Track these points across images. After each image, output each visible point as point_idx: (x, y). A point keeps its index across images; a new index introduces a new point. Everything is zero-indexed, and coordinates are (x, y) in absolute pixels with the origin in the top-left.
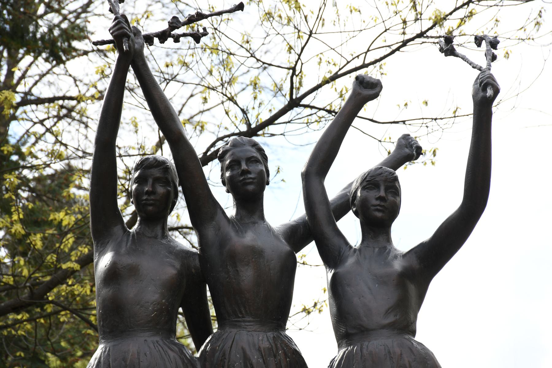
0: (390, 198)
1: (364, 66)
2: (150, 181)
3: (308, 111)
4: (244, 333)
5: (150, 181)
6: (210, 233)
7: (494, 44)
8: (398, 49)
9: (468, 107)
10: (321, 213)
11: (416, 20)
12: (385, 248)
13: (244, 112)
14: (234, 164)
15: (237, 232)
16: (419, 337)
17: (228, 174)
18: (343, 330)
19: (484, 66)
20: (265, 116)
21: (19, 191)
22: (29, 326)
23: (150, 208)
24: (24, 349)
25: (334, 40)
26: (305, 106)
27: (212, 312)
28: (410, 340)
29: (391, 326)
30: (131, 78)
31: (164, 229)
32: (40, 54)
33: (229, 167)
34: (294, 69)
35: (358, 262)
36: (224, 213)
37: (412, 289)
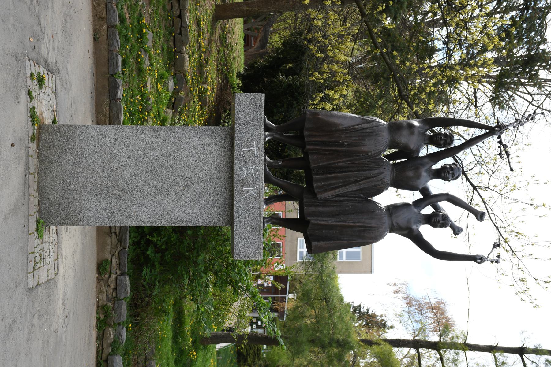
0: (439, 225)
1: (489, 213)
2: (445, 139)
3: (471, 192)
4: (390, 173)
5: (445, 139)
6: (426, 160)
7: (497, 262)
8: (495, 225)
9: (473, 253)
10: (434, 200)
11: (506, 232)
12: (420, 223)
13: (471, 169)
14: (452, 169)
15: (426, 170)
16: (388, 234)
17: (448, 166)
18: (391, 208)
19: (488, 259)
20: (469, 177)
22: (393, 94)
23: (435, 139)
24: (385, 93)
25: (499, 202)
26: (473, 192)
27: (398, 161)
28: (388, 231)
29: (392, 225)
30: (484, 131)
31: (427, 144)
32: (493, 93)
33: (450, 167)
34: (488, 188)
35: (415, 213)
36: (433, 165)
37: (406, 232)
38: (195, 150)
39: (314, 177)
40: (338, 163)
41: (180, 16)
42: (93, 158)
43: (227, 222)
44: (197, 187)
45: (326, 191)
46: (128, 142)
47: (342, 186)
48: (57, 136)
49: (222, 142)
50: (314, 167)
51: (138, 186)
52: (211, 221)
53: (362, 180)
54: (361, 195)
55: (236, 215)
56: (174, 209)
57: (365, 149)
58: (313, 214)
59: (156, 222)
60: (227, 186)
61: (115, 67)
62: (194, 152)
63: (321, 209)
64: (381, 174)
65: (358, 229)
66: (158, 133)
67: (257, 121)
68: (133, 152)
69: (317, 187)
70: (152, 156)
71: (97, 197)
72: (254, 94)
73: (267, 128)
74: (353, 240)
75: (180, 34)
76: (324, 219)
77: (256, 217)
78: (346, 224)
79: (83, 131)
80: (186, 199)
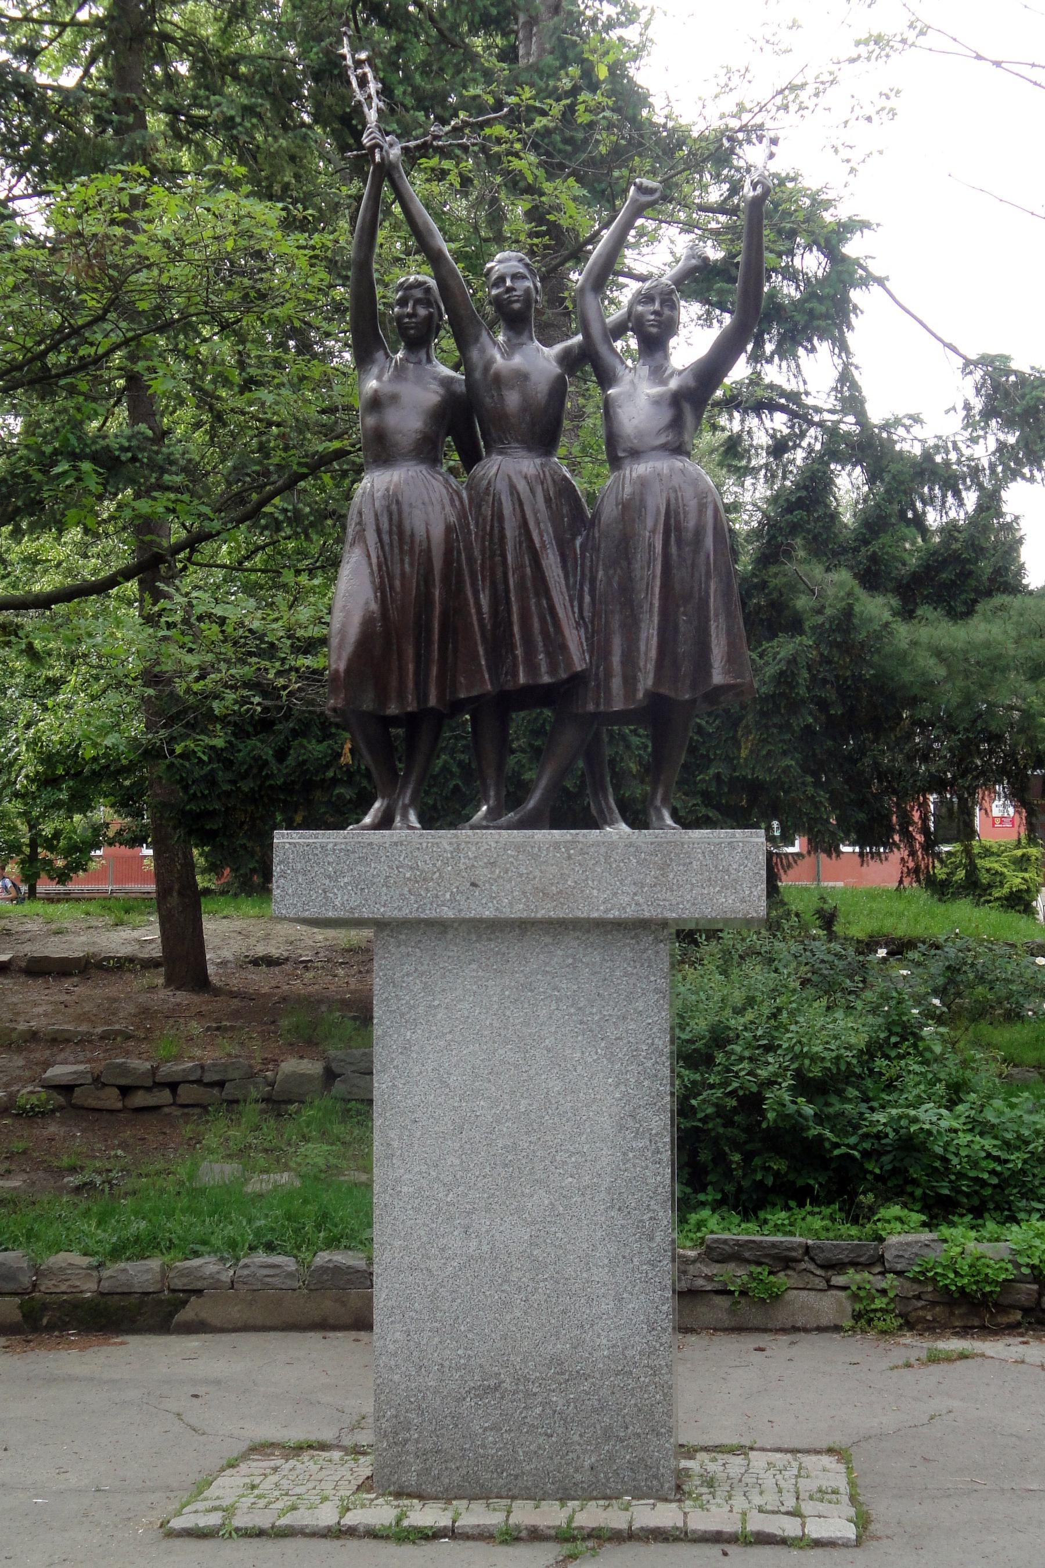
0: (667, 312)
21: (317, 214)
23: (412, 332)
29: (664, 447)
37: (687, 409)
38: (444, 1034)
39: (522, 680)
40: (479, 611)
41: (173, 1086)
42: (470, 1336)
43: (656, 938)
44: (553, 1029)
45: (564, 647)
46: (423, 1233)
47: (549, 599)
48: (406, 1441)
49: (419, 954)
50: (492, 684)
51: (551, 1203)
52: (653, 986)
53: (530, 540)
54: (578, 542)
55: (630, 913)
56: (618, 1095)
57: (438, 532)
58: (630, 681)
59: (657, 1151)
60: (548, 940)
61: (277, 1271)
62: (449, 1037)
63: (616, 660)
64: (513, 488)
65: (674, 550)
66: (395, 1144)
67: (354, 852)
68: (451, 1218)
69: (553, 670)
70: (462, 1162)
71: (587, 1327)
72: (276, 861)
73: (385, 822)
74: (708, 564)
75: (221, 1084)
76: (643, 648)
77: (637, 850)
78: (658, 583)
79: (393, 1363)
80: (590, 1060)
